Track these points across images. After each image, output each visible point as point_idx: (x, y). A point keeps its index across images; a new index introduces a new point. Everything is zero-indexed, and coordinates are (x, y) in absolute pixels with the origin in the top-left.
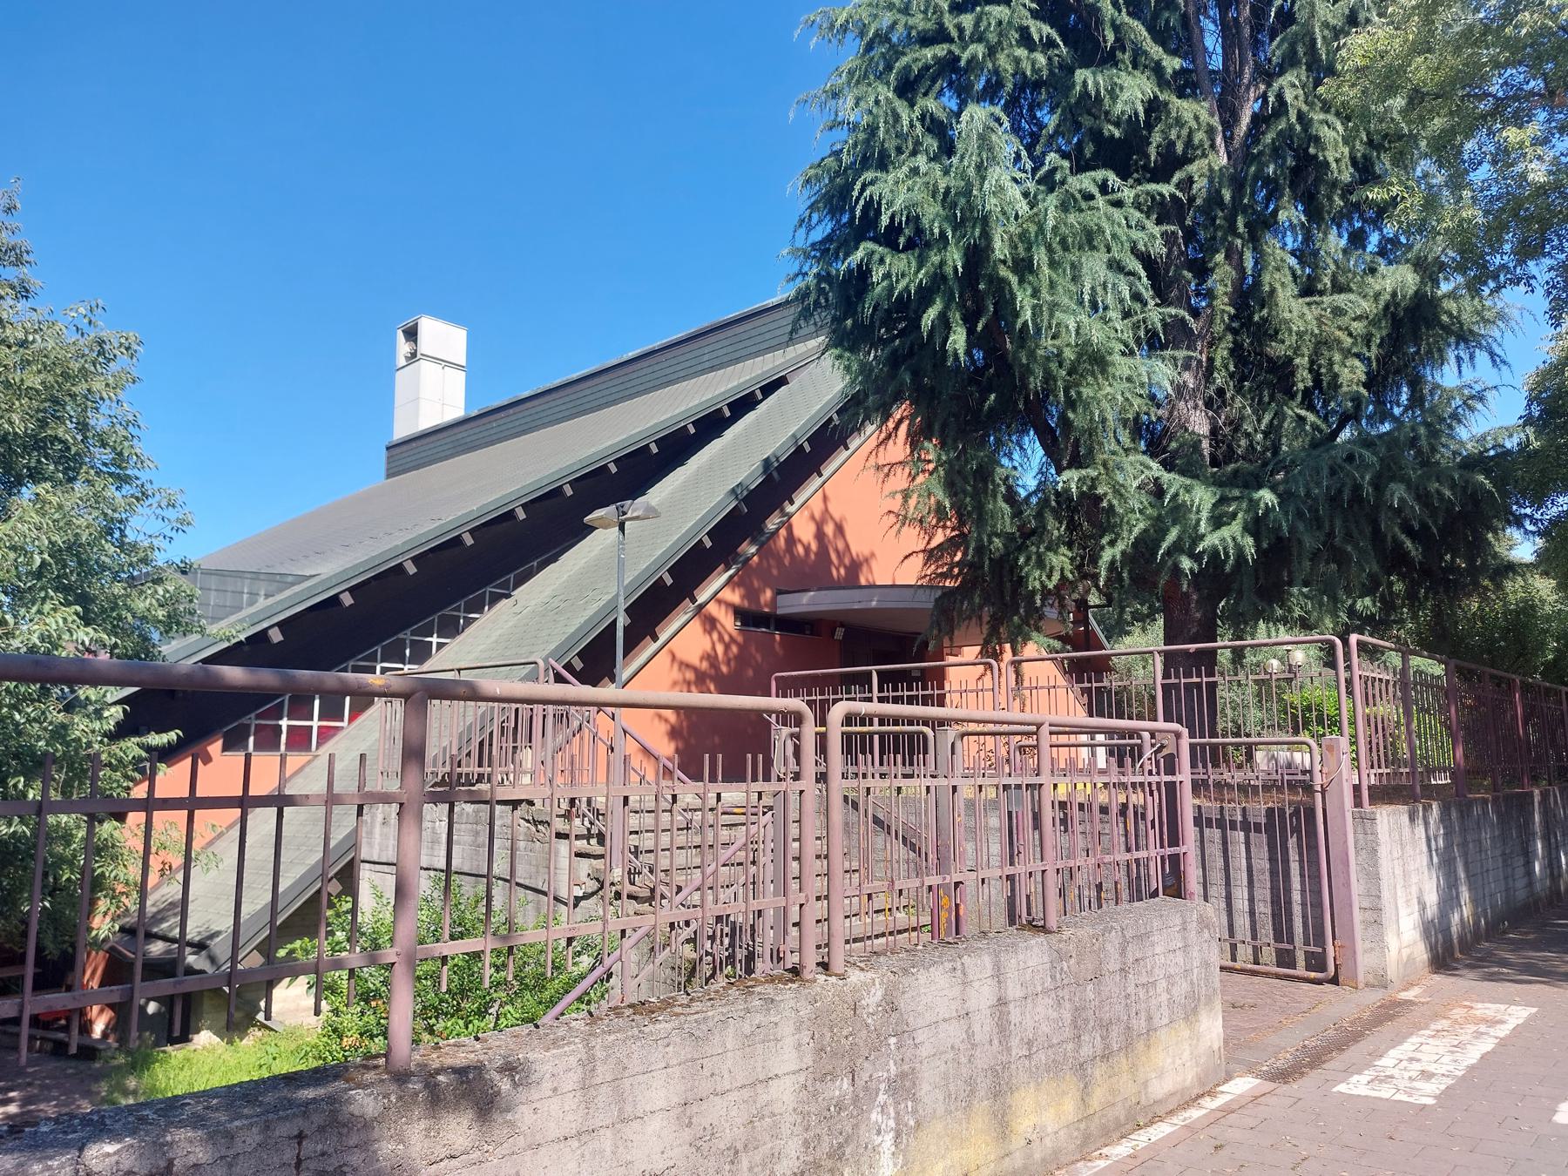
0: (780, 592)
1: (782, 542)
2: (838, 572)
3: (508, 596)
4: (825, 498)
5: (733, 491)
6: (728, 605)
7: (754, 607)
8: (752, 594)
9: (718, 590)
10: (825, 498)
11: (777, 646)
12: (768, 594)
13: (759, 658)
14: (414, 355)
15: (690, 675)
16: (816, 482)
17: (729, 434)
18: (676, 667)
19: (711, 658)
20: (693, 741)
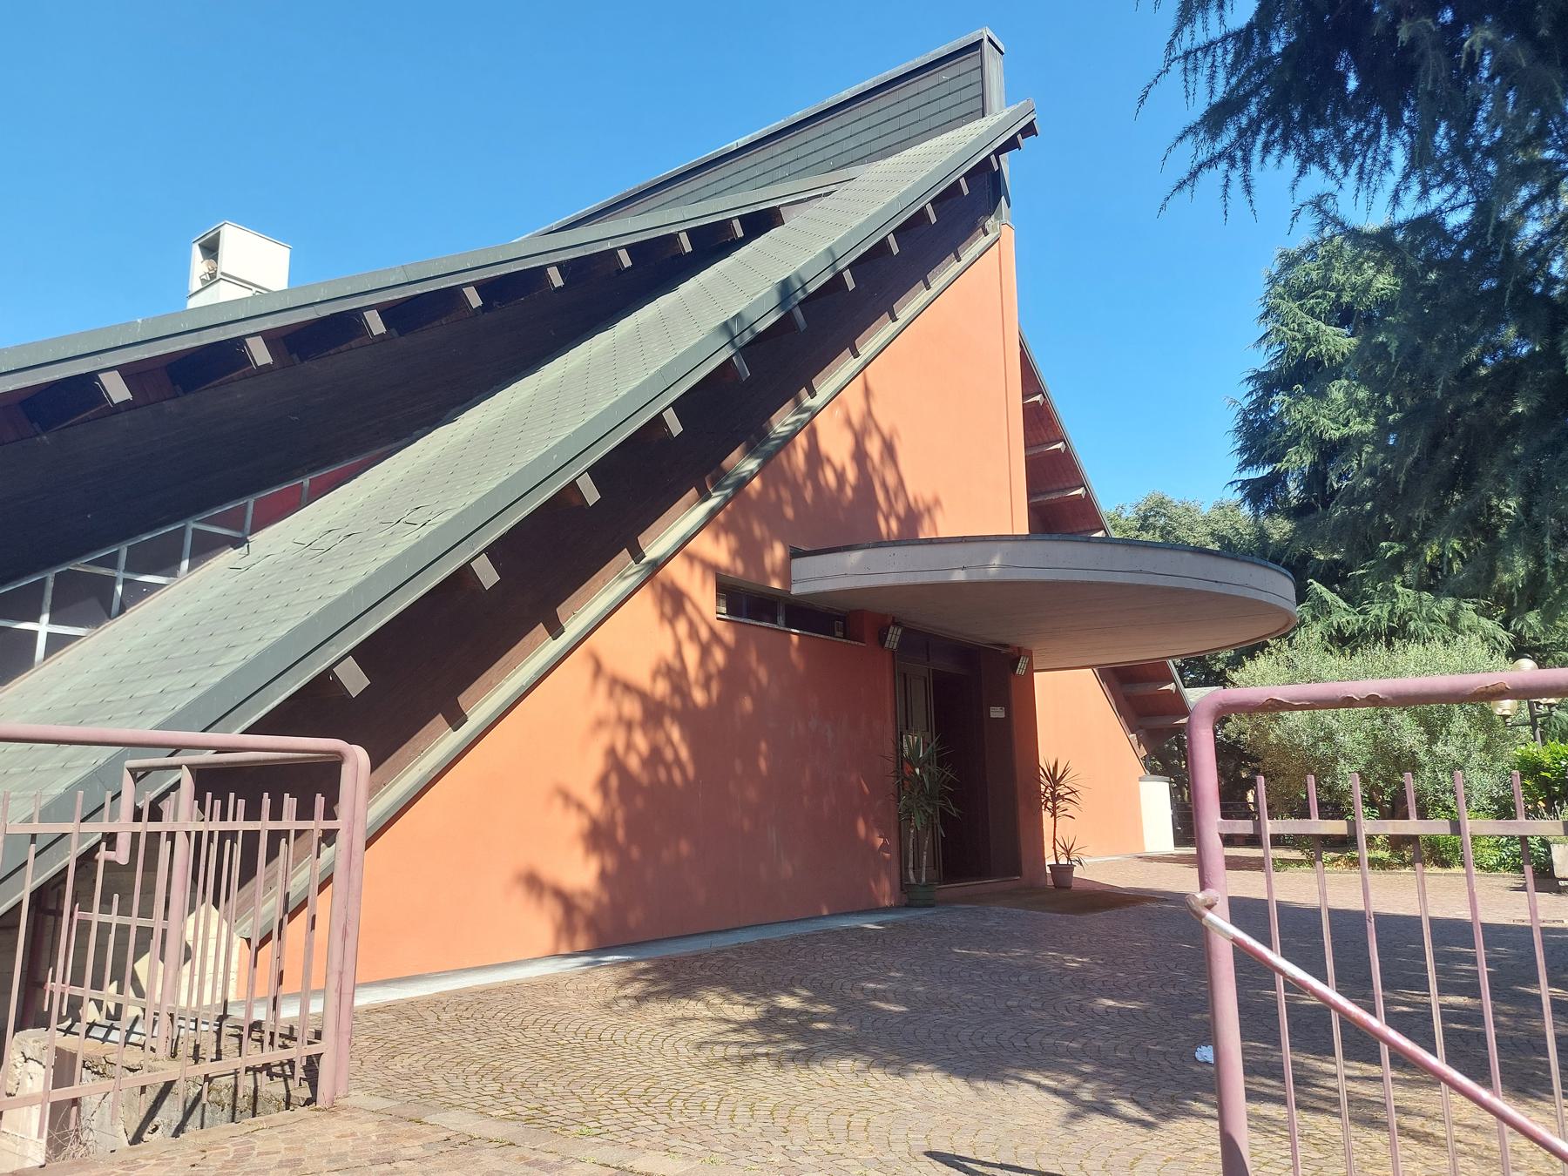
0: (795, 554)
1: (799, 458)
2: (889, 526)
3: (237, 543)
4: (867, 391)
5: (726, 326)
6: (710, 567)
7: (753, 577)
8: (749, 550)
9: (683, 531)
10: (867, 391)
11: (794, 655)
12: (779, 551)
13: (763, 674)
14: (213, 276)
15: (632, 708)
16: (845, 366)
17: (687, 288)
18: (602, 688)
19: (674, 674)
20: (635, 853)
